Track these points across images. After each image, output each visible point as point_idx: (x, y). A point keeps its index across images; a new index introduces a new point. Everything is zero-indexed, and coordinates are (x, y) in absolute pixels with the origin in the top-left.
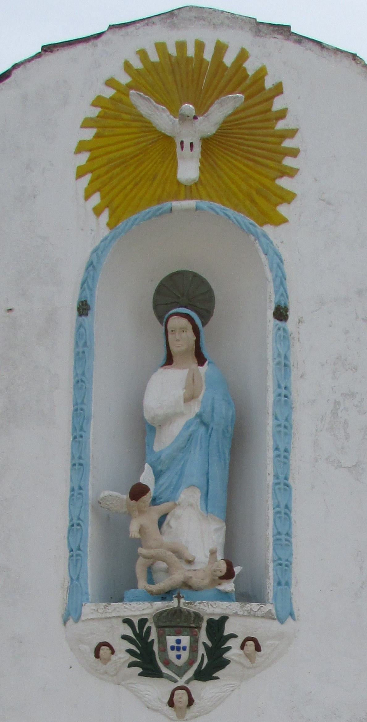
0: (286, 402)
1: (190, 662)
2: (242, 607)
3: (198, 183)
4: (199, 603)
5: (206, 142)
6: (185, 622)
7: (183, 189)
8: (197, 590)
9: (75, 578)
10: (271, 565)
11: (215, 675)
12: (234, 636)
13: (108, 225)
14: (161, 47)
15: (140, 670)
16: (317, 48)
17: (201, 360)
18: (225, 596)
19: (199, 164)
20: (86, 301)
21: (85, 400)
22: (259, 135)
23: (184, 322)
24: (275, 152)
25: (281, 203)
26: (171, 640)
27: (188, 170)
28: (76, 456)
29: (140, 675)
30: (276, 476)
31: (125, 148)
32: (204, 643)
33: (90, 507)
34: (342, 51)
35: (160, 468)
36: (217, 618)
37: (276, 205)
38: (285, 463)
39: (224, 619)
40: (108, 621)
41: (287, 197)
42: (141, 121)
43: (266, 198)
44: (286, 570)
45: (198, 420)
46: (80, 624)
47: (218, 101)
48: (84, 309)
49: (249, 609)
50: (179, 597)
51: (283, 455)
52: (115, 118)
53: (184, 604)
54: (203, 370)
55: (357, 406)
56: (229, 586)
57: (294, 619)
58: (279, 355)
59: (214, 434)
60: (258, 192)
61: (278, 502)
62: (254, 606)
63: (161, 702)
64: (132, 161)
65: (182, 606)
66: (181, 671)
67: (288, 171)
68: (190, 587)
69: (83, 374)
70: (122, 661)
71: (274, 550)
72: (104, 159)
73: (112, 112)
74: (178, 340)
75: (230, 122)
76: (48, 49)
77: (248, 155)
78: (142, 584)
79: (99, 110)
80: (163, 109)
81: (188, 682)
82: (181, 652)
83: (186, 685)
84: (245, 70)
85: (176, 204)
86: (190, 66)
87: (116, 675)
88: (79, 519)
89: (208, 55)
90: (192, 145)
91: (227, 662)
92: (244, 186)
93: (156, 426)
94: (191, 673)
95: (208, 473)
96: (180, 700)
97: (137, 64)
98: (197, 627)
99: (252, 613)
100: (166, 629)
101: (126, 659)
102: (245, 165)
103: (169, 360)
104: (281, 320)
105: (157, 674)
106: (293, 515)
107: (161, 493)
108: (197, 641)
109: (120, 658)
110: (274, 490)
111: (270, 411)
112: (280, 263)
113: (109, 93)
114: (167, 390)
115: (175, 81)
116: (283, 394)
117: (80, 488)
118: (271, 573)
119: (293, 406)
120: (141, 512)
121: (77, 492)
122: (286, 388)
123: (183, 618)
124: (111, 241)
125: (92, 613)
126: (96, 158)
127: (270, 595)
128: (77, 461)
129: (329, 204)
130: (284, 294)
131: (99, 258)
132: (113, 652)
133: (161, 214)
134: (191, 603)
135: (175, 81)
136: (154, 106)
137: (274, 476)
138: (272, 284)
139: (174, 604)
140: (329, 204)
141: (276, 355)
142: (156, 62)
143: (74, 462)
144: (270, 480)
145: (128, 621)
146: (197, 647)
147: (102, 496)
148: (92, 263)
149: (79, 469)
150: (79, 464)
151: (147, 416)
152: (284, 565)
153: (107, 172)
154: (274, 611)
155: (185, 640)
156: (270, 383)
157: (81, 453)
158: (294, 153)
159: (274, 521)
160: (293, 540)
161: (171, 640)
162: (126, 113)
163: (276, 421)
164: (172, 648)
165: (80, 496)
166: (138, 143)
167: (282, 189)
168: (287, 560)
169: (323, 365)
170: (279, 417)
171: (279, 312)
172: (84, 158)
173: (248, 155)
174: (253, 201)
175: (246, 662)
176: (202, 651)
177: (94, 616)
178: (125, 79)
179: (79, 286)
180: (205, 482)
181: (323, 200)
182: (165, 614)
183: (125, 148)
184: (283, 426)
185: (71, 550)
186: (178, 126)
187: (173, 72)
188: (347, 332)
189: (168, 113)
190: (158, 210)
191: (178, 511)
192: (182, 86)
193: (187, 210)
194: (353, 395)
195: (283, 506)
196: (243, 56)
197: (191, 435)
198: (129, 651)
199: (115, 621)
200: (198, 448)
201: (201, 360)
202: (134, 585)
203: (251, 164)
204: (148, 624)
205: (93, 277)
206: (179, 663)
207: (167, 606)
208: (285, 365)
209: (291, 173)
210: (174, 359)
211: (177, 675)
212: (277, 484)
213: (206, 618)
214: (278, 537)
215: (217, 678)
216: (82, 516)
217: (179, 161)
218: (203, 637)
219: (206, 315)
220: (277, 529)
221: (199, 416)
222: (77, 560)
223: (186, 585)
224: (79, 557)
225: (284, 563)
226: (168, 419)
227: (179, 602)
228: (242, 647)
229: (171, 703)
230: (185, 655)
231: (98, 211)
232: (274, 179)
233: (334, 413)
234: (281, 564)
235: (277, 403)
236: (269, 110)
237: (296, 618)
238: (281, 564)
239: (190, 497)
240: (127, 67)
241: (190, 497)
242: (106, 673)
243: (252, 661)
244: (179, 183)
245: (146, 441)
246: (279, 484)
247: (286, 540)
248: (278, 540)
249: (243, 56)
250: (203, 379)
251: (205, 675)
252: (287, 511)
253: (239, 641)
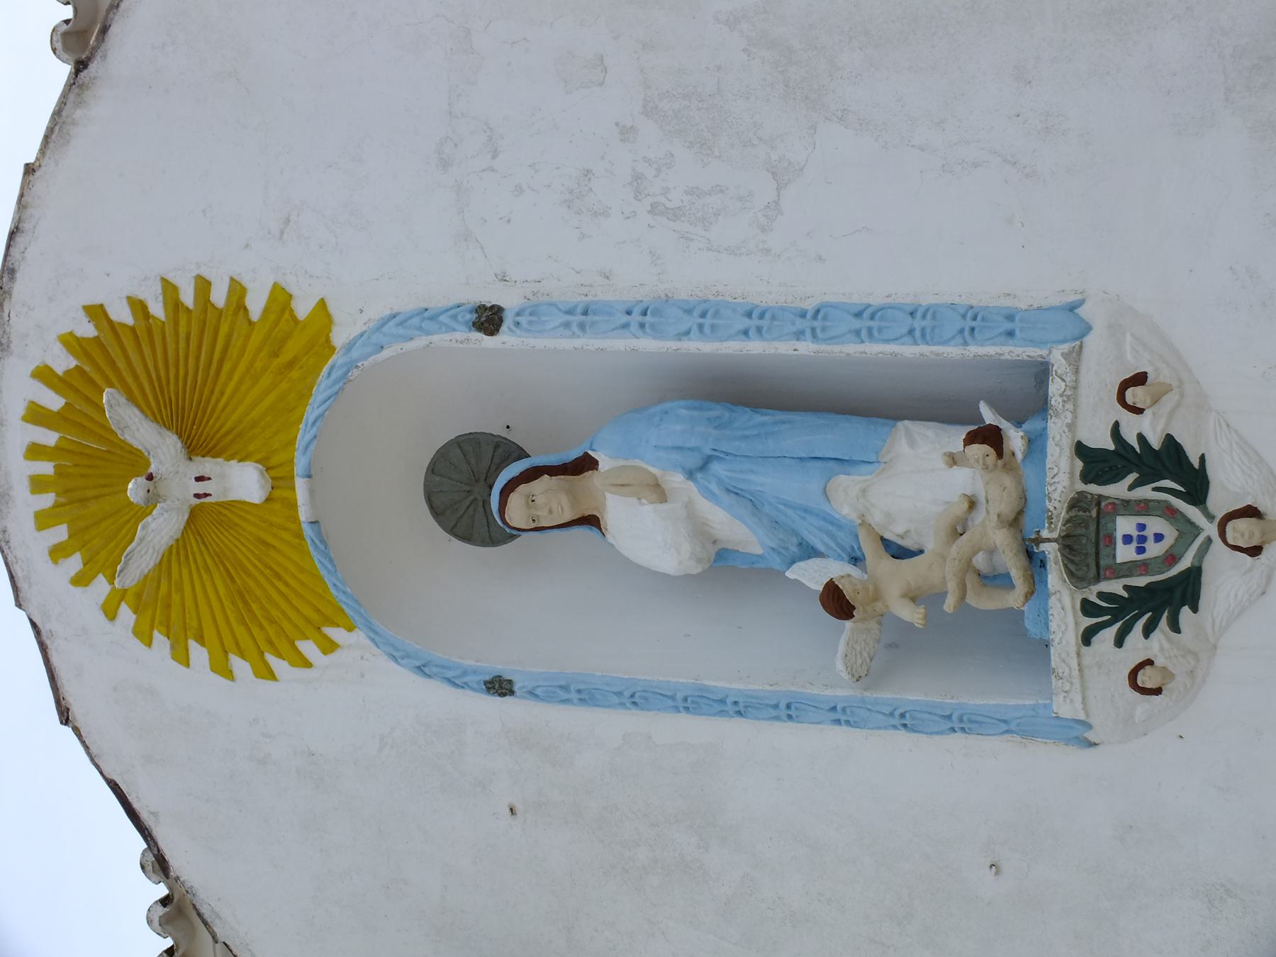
0: (657, 312)
1: (1170, 513)
3: (268, 466)
4: (1050, 500)
5: (194, 448)
6: (1087, 527)
7: (277, 493)
8: (1024, 498)
9: (1004, 727)
10: (973, 350)
11: (1196, 463)
13: (350, 630)
14: (43, 520)
15: (1186, 611)
16: (19, 239)
17: (585, 464)
18: (1035, 444)
19: (233, 462)
20: (486, 683)
21: (668, 693)
22: (177, 350)
23: (515, 499)
24: (204, 323)
25: (292, 311)
26: (1125, 553)
27: (243, 482)
28: (773, 713)
29: (1195, 609)
30: (799, 335)
31: (217, 591)
32: (1131, 488)
33: (867, 694)
34: (21, 196)
35: (794, 549)
36: (1079, 464)
37: (296, 321)
38: (773, 318)
39: (1081, 450)
40: (1090, 672)
41: (280, 300)
42: (169, 561)
43: (283, 342)
44: (983, 319)
45: (699, 475)
46: (1092, 721)
47: (119, 432)
48: (501, 687)
49: (1060, 400)
50: (1039, 540)
51: (758, 319)
52: (168, 606)
53: (1051, 531)
54: (605, 463)
55: (659, 170)
56: (1015, 439)
57: (1082, 302)
58: (567, 325)
59: (725, 446)
60: (276, 354)
61: (850, 332)
62: (1055, 388)
63: (1251, 570)
64: (239, 582)
65: (1055, 535)
66: (1188, 530)
67: (235, 298)
68: (1021, 512)
69: (619, 694)
70: (1166, 645)
71: (945, 343)
72: (240, 630)
73: (158, 612)
74: (551, 512)
75: (153, 414)
76: (65, 717)
77: (212, 372)
78: (1014, 599)
79: (156, 633)
80: (143, 528)
81: (1210, 517)
82: (1149, 533)
83: (1217, 520)
84: (67, 372)
85: (304, 514)
86: (70, 470)
87: (1196, 656)
88: (892, 714)
89: (50, 438)
90: (199, 479)
91: (1170, 440)
92: (266, 381)
93: (712, 550)
94: (1192, 512)
95: (801, 459)
96: (1247, 536)
97: (74, 563)
98: (1099, 504)
99: (1068, 393)
100: (1102, 563)
101: (1162, 636)
102: (230, 378)
103: (591, 521)
104: (501, 320)
105: (1193, 578)
106: (877, 300)
107: (843, 549)
108: (1126, 503)
109: (1162, 649)
110: (825, 341)
111: (672, 345)
112: (398, 319)
113: (126, 614)
114: (644, 532)
115: (97, 497)
116: (640, 318)
117: (834, 709)
118: (991, 350)
119: (663, 297)
120: (877, 596)
121: (839, 714)
122: (629, 313)
123: (1080, 531)
124: (376, 633)
125: (1072, 701)
126: (237, 644)
127: (1033, 354)
128: (783, 712)
129: (287, 221)
130: (450, 313)
131: (407, 656)
132: (1149, 662)
133: (323, 541)
134: (1050, 518)
135: (97, 497)
136: (139, 544)
137: (798, 339)
138: (435, 338)
139: (1051, 551)
140: (287, 221)
141: (568, 333)
142: (69, 530)
143: (785, 718)
144: (806, 348)
146: (1138, 502)
147: (845, 676)
148: (419, 668)
149: (797, 709)
150: (789, 710)
151: (696, 569)
152: (974, 324)
153: (261, 627)
154: (1066, 347)
155: (1125, 525)
156: (620, 344)
157: (767, 705)
158: (203, 286)
159: (887, 341)
160: (926, 301)
161: (1125, 553)
162: (158, 587)
163: (692, 335)
164: (1141, 550)
165: (848, 711)
166: (207, 568)
167: (266, 310)
168: (964, 316)
169: (583, 236)
170: (684, 328)
171: (486, 325)
172: (239, 665)
173: (212, 372)
174: (290, 365)
175: (1169, 401)
176: (1146, 492)
177: (1078, 698)
178: (101, 587)
179: (460, 691)
180: (819, 464)
181: (282, 233)
182: (1072, 567)
183: (217, 591)
184: (701, 320)
185: (953, 730)
186: (168, 502)
187: (83, 501)
188: (519, 190)
189: (149, 518)
190: (316, 547)
191: (876, 518)
192: (105, 486)
193: (312, 493)
194: (638, 178)
195: (857, 324)
196: (44, 375)
197: (728, 490)
198: (1147, 631)
199: (1087, 661)
200: (752, 477)
201: (585, 464)
202: (1015, 616)
203: (227, 367)
204: (1094, 599)
205: (443, 667)
206: (1170, 534)
207: (1056, 563)
208: (585, 313)
209: (237, 290)
211: (1197, 536)
212: (814, 336)
213: (1081, 486)
214: (918, 334)
216: (887, 710)
217: (232, 496)
218: (1118, 490)
219: (509, 451)
220: (902, 337)
221: (690, 475)
222: (970, 721)
223: (1015, 522)
224: (965, 718)
225: (969, 323)
226: (700, 531)
227: (1049, 540)
228: (1138, 411)
229: (1255, 551)
230: (1155, 524)
231: (329, 647)
232: (250, 323)
233: (675, 214)
234: (973, 329)
235: (657, 332)
236: (133, 329)
237: (1079, 297)
238: (973, 329)
239: (848, 496)
240: (81, 580)
241: (848, 496)
242: (1192, 673)
243: (1167, 389)
244: (268, 500)
246: (813, 330)
247: (924, 317)
248: (923, 335)
249: (44, 375)
250: (621, 463)
251: (1195, 484)
252: (866, 314)
253: (1126, 418)
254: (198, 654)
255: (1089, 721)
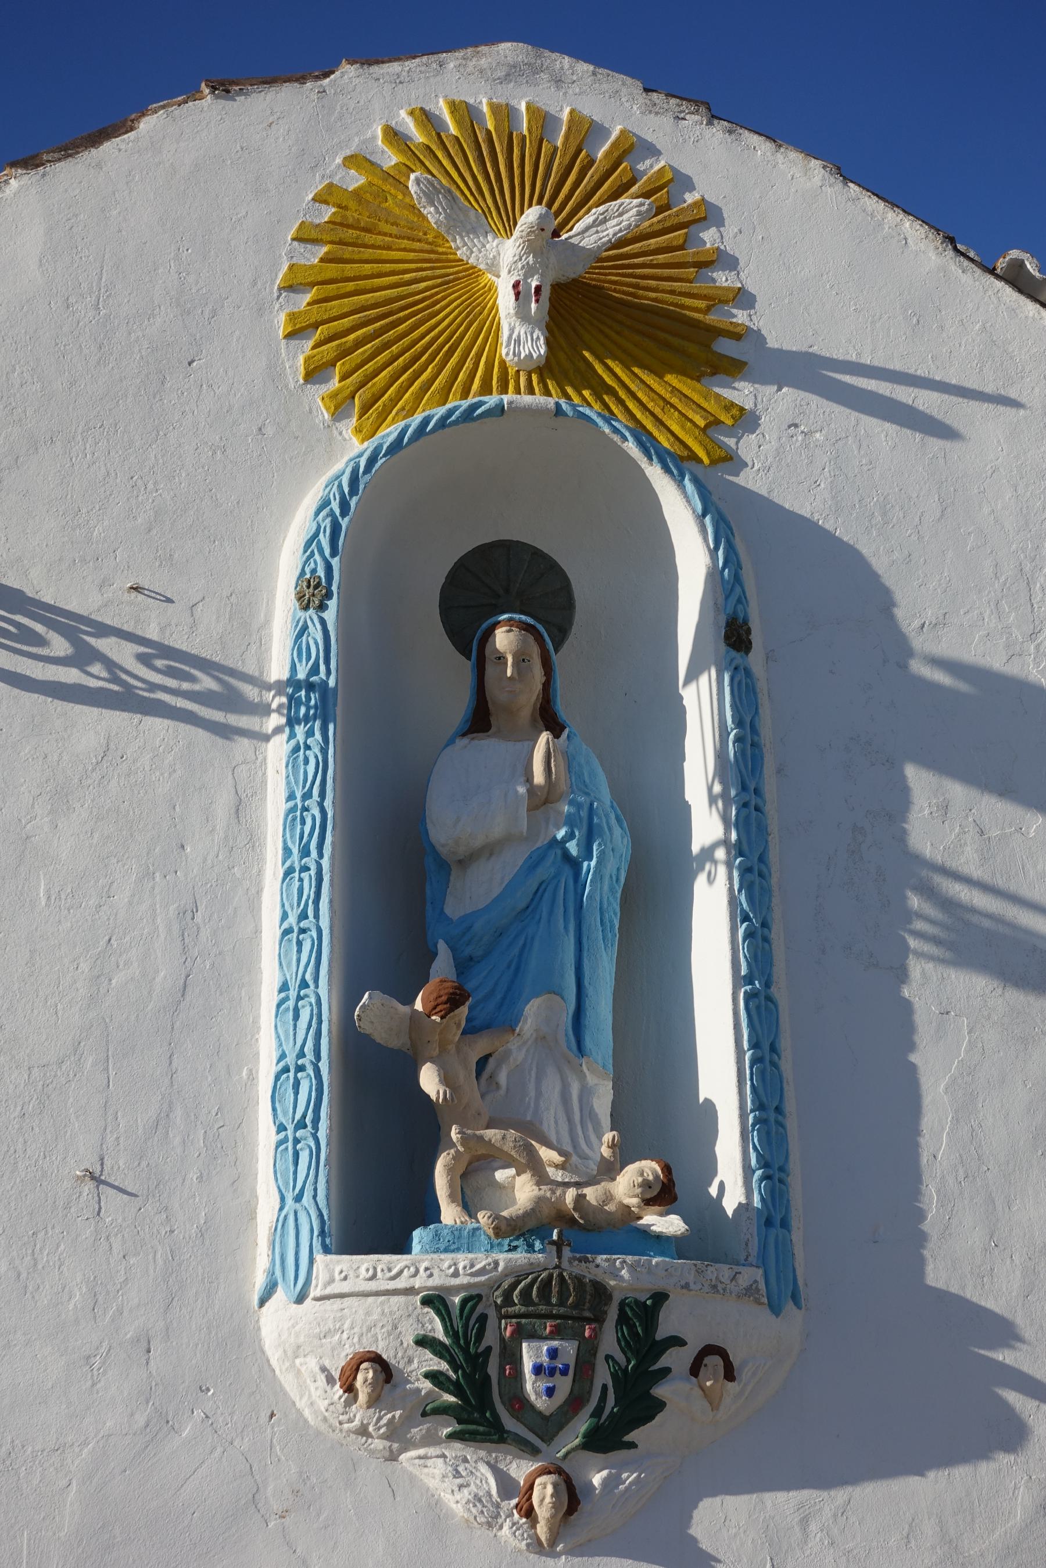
1: (574, 1403)
2: (699, 1272)
12: (677, 1341)
35: (468, 951)
66: (548, 1427)
94: (582, 1425)
108: (593, 1352)
113: (355, 180)
145: (435, 1301)
146: (592, 1366)
176: (603, 1375)
210: (493, 720)
215: (632, 1445)
218: (609, 1342)
228: (695, 1370)
245: (428, 892)
254: (314, 255)
255: (308, 1301)
